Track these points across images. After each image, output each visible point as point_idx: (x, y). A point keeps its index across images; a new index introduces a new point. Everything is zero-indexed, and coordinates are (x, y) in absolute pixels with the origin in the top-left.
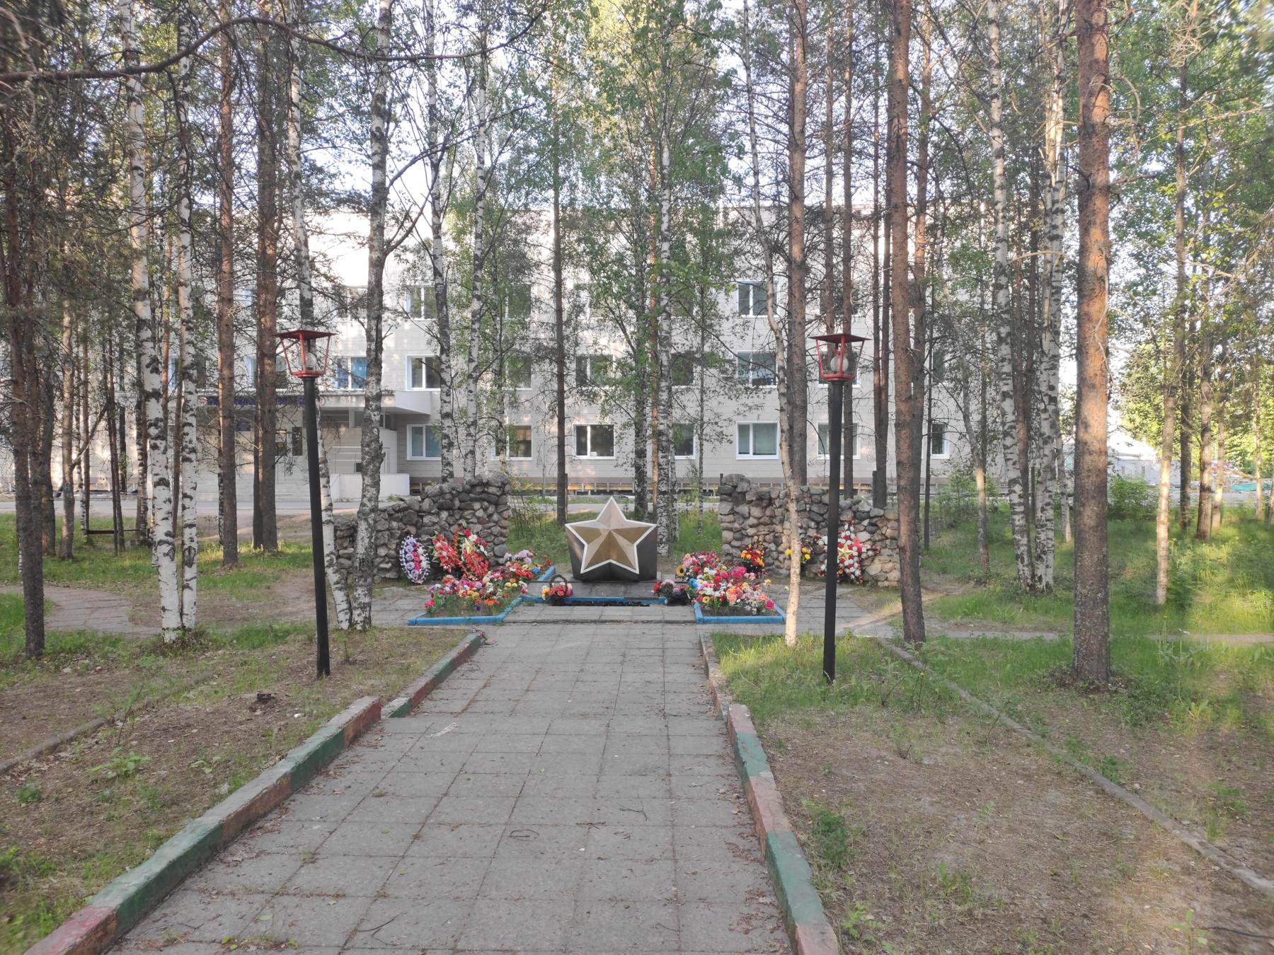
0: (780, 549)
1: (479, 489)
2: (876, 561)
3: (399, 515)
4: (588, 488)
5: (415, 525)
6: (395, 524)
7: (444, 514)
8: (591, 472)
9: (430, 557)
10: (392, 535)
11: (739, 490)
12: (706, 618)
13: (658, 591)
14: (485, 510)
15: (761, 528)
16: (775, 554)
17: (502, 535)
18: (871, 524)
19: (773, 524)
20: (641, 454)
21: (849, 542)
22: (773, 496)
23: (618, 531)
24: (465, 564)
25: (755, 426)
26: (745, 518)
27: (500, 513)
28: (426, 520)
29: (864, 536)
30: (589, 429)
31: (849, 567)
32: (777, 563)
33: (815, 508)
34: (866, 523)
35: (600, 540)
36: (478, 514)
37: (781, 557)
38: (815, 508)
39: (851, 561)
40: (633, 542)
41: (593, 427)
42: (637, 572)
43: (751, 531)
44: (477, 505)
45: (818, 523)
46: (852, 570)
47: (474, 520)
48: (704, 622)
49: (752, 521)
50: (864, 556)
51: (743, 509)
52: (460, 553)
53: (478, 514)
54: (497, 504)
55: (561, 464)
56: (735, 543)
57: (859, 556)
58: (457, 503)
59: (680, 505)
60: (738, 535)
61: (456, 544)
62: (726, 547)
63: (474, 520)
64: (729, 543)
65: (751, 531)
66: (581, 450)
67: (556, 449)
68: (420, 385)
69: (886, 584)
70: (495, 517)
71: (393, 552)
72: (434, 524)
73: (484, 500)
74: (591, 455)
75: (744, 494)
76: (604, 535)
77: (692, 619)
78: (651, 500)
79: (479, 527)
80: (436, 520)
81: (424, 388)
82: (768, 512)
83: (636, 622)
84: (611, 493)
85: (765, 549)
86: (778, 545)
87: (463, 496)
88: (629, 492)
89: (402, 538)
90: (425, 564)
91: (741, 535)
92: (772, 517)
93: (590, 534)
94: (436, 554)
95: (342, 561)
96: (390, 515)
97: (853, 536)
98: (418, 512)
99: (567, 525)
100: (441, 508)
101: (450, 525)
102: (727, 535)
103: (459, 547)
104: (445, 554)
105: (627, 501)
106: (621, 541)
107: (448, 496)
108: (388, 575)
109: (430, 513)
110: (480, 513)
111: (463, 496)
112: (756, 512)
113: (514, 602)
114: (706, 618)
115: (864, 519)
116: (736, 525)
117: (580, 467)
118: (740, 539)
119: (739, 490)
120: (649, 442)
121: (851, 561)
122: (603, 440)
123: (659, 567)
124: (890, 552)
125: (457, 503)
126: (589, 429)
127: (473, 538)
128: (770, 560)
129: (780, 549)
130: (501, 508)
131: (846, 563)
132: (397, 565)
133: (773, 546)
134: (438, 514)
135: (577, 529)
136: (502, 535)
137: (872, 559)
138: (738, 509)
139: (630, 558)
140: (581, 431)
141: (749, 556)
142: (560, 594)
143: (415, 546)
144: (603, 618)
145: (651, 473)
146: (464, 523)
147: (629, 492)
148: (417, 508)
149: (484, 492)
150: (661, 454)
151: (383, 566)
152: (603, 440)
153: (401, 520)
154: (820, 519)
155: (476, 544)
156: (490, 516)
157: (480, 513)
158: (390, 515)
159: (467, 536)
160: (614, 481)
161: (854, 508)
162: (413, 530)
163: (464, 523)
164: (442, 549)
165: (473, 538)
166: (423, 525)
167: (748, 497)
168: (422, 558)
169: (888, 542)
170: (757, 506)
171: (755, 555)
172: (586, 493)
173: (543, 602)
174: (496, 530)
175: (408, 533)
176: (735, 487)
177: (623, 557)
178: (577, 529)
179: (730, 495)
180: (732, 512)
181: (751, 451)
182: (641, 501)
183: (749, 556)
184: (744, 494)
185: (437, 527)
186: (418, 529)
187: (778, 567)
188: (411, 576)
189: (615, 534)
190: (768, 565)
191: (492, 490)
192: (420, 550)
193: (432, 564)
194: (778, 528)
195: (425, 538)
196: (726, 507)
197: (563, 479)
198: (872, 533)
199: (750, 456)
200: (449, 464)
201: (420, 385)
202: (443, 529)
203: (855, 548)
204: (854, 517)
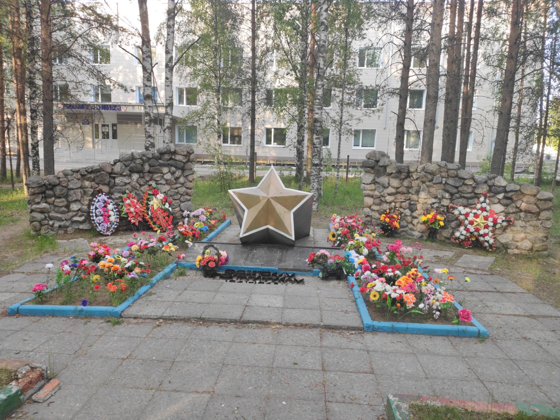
0: (415, 214)
1: (167, 157)
2: (508, 231)
3: (92, 176)
4: (272, 162)
5: (108, 184)
6: (87, 183)
7: (135, 176)
8: (273, 154)
9: (120, 212)
10: (85, 193)
11: (381, 164)
12: (376, 324)
13: (313, 262)
14: (173, 173)
15: (399, 196)
16: (409, 219)
17: (187, 194)
18: (505, 198)
19: (409, 193)
20: (300, 142)
21: (485, 213)
22: (412, 170)
23: (276, 199)
24: (151, 218)
25: (364, 131)
26: (385, 187)
27: (186, 177)
28: (118, 180)
29: (498, 208)
30: (273, 130)
31: (484, 235)
32: (410, 226)
33: (451, 181)
34: (501, 196)
35: (259, 207)
36: (166, 177)
37: (415, 222)
38: (451, 181)
39: (486, 231)
40: (290, 209)
41: (275, 129)
42: (293, 238)
43: (389, 199)
44: (165, 170)
45: (452, 195)
46: (487, 238)
47: (163, 182)
48: (374, 330)
49: (391, 190)
50: (498, 226)
51: (384, 180)
52: (148, 209)
53: (166, 177)
54: (183, 169)
55: (252, 146)
56: (375, 208)
57: (494, 226)
58: (147, 167)
59: (323, 174)
60: (377, 201)
61: (145, 201)
62: (367, 210)
63: (163, 182)
64: (370, 207)
65: (389, 199)
66: (268, 141)
67: (249, 137)
68: (183, 104)
69: (516, 251)
70: (182, 180)
71: (85, 207)
72: (126, 184)
73: (172, 166)
74: (273, 144)
75: (385, 167)
76: (263, 202)
77: (357, 324)
78: (305, 170)
79: (167, 188)
80: (127, 181)
81: (185, 104)
82: (406, 183)
83: (287, 325)
84: (284, 165)
85: (401, 213)
86: (412, 211)
87: (153, 162)
88: (293, 165)
89: (94, 195)
90: (113, 218)
91: (381, 200)
92: (409, 187)
93: (250, 201)
94: (125, 209)
95: (35, 214)
96: (83, 176)
97: (488, 208)
98: (110, 174)
99: (230, 191)
100: (132, 171)
101: (141, 186)
102: (369, 201)
103: (147, 204)
104: (132, 209)
105: (292, 170)
106: (279, 208)
107: (138, 161)
108: (81, 227)
109: (121, 175)
110: (168, 176)
111: (153, 162)
112: (395, 183)
113: (154, 280)
114: (376, 324)
115: (499, 193)
116: (376, 193)
117: (267, 150)
118: (379, 204)
119: (381, 164)
120: (306, 131)
121: (486, 231)
122: (281, 136)
123: (314, 220)
124: (523, 224)
125: (147, 167)
126: (273, 130)
127: (161, 196)
128: (404, 223)
129: (415, 214)
130: (187, 173)
131: (482, 232)
132: (88, 218)
133: (408, 212)
134: (130, 176)
135: (240, 195)
136: (187, 194)
137: (504, 229)
138: (378, 180)
139: (287, 225)
140: (268, 131)
141: (387, 220)
142: (212, 265)
143: (105, 202)
144: (248, 316)
145: (307, 154)
146: (153, 184)
147: (293, 165)
148: (109, 170)
149: (171, 159)
150: (315, 136)
151: (75, 219)
152: (281, 136)
153: (93, 180)
154: (455, 190)
155: (164, 201)
156: (177, 179)
157: (168, 176)
158: (83, 176)
159: (155, 194)
160: (286, 159)
161: (490, 183)
162: (105, 189)
163: (153, 184)
164: (131, 206)
165: (161, 196)
166: (115, 185)
167: (389, 170)
168: (111, 213)
169: (522, 214)
170: (396, 177)
171: (392, 218)
172: (270, 165)
173: (197, 269)
174: (182, 190)
175: (100, 191)
176: (377, 161)
177: (280, 224)
178: (240, 195)
179: (373, 168)
180: (374, 182)
181: (361, 144)
182: (299, 170)
183: (387, 220)
184: (385, 167)
185: (128, 186)
186: (111, 188)
187: (411, 229)
188: (99, 228)
189: (272, 201)
190: (402, 227)
191: (178, 157)
192: (110, 207)
193: (121, 219)
194: (414, 197)
195: (117, 195)
196: (368, 178)
197: (253, 156)
198: (506, 205)
199: (360, 147)
200: (150, 136)
201: (183, 104)
202: (134, 188)
203: (491, 219)
204: (490, 191)
